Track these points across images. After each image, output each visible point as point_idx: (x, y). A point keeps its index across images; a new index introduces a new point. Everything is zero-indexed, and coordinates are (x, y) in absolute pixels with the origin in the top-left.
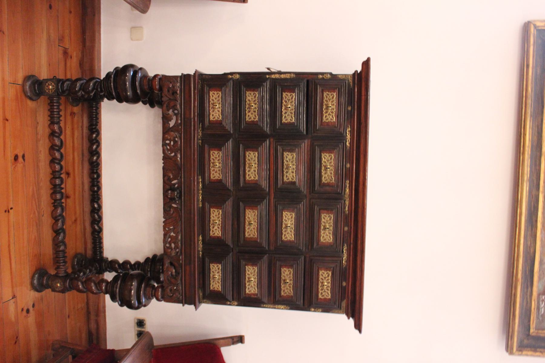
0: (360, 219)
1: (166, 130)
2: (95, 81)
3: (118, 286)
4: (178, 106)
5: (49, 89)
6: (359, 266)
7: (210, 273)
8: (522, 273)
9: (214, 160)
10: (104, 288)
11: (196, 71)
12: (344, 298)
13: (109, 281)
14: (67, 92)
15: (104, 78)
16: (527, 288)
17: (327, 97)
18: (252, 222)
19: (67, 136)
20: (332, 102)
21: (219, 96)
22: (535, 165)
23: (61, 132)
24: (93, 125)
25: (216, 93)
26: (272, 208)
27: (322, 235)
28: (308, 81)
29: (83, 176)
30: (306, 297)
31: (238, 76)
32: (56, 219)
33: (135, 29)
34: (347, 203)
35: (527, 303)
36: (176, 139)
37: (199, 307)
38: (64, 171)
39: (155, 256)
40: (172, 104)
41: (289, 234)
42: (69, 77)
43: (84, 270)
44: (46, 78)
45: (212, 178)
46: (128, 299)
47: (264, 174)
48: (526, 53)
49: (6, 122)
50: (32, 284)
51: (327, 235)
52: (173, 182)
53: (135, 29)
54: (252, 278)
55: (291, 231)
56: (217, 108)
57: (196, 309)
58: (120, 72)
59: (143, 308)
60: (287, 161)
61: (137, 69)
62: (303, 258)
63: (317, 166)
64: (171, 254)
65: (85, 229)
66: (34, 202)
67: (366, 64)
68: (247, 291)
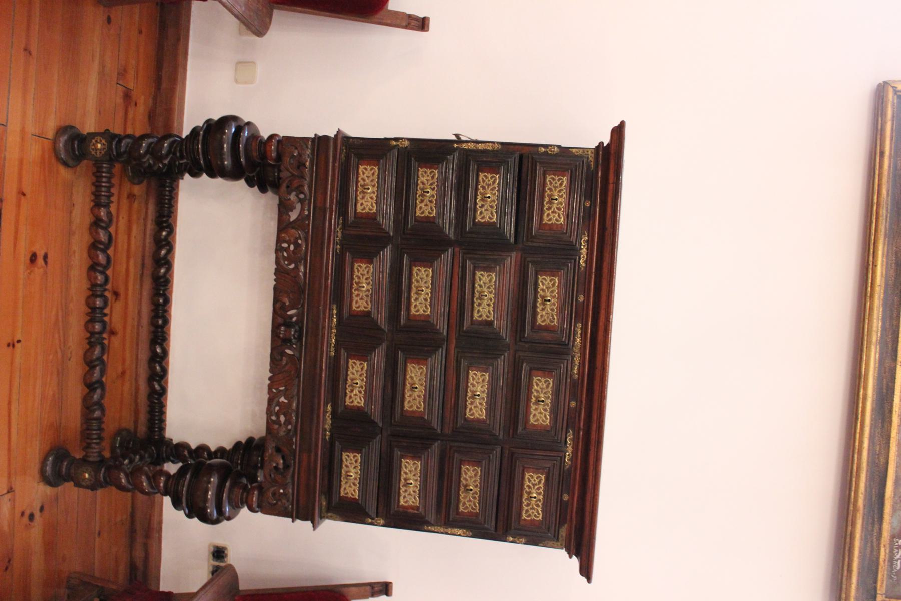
0: (597, 388)
1: (283, 226)
2: (171, 139)
3: (186, 483)
4: (306, 188)
5: (96, 149)
6: (591, 468)
7: (341, 467)
8: (865, 500)
9: (359, 278)
10: (162, 485)
11: (339, 132)
12: (565, 523)
13: (172, 474)
14: (125, 157)
15: (187, 137)
16: (873, 524)
17: (551, 183)
18: (417, 384)
19: (118, 252)
20: (559, 191)
21: (373, 174)
22: (891, 318)
23: (110, 221)
24: (164, 217)
25: (369, 168)
26: (452, 363)
27: (533, 412)
28: (521, 157)
29: (140, 300)
30: (501, 518)
31: (407, 143)
32: (90, 364)
33: (243, 65)
34: (577, 360)
35: (872, 552)
36: (300, 242)
37: (319, 524)
38: (109, 287)
39: (250, 440)
40: (296, 183)
41: (476, 409)
42: (129, 131)
43: (132, 455)
44: (92, 130)
45: (354, 308)
46: (201, 505)
47: (443, 309)
48: (879, 133)
49: (22, 197)
50: (42, 472)
51: (541, 413)
52: (289, 313)
53: (243, 65)
54: (411, 475)
55: (480, 404)
56: (369, 193)
57: (315, 527)
58: (214, 128)
59: (225, 522)
60: (481, 286)
61: (242, 124)
62: (498, 450)
63: (530, 297)
64: (278, 433)
65: (137, 389)
66: (56, 336)
67: (618, 132)
68: (402, 502)
